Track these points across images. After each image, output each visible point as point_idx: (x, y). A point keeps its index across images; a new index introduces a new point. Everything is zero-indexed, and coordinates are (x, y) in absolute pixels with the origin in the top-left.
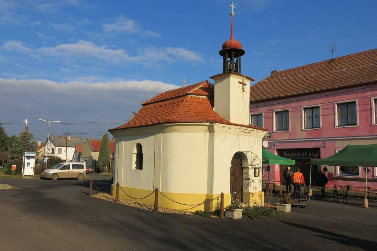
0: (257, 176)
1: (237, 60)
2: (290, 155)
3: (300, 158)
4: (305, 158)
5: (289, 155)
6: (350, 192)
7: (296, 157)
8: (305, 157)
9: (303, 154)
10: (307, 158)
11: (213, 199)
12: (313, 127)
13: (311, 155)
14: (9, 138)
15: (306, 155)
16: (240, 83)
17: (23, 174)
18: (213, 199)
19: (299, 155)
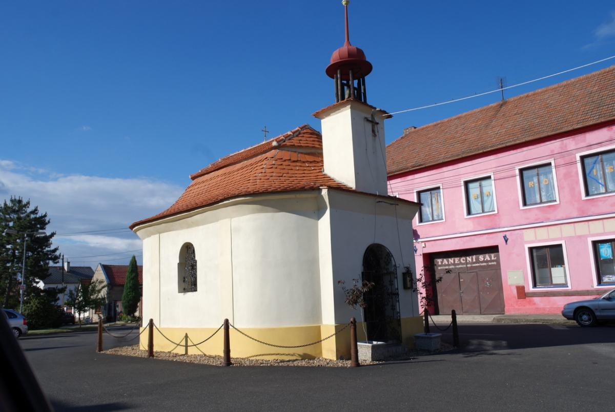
0: (409, 288)
1: (359, 84)
2: (448, 261)
3: (465, 266)
4: (473, 265)
5: (447, 263)
6: (413, 284)
7: (458, 264)
8: (474, 263)
9: (469, 259)
10: (477, 265)
11: (322, 339)
12: (483, 212)
13: (482, 259)
14: (540, 308)
15: (474, 261)
16: (367, 120)
17: (587, 293)
18: (322, 339)
19: (463, 260)
